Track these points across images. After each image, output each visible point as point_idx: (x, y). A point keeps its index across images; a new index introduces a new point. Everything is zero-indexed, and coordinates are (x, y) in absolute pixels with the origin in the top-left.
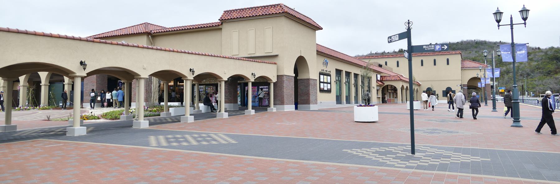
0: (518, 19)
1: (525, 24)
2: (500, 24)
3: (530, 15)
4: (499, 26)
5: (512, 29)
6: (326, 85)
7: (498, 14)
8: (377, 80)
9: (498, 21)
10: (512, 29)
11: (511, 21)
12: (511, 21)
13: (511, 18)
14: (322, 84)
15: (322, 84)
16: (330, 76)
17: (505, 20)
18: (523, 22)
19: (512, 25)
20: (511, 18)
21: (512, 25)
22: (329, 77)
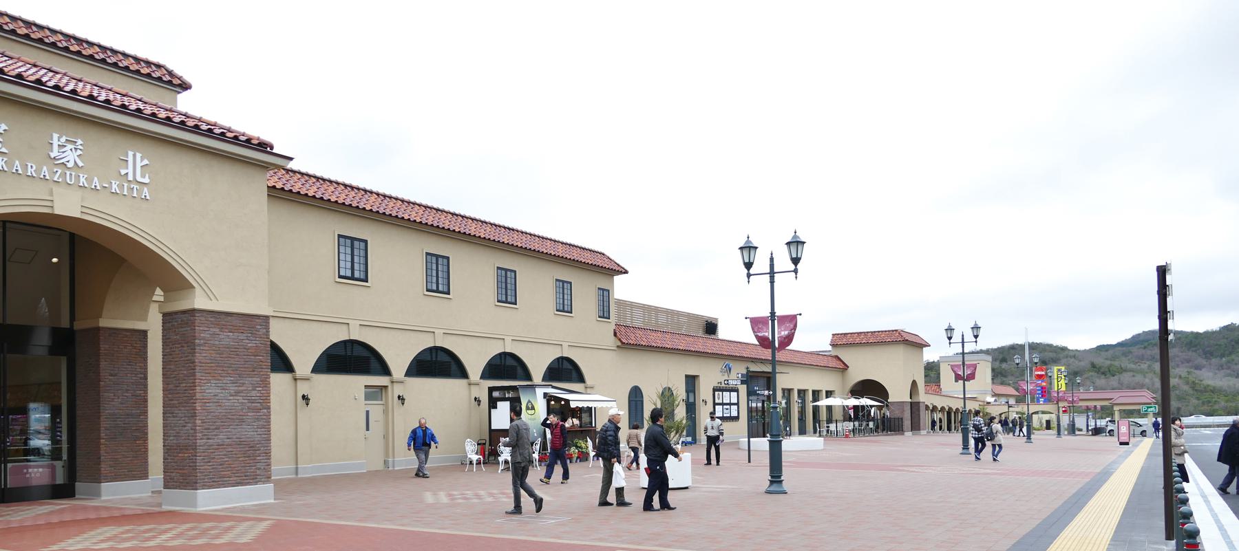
0: (783, 262)
1: (796, 271)
2: (752, 271)
3: (807, 254)
4: (749, 275)
5: (772, 282)
6: (726, 401)
7: (950, 330)
8: (816, 395)
9: (950, 338)
10: (772, 282)
11: (772, 266)
12: (772, 266)
13: (772, 259)
14: (734, 400)
15: (734, 400)
16: (737, 391)
17: (761, 264)
18: (792, 267)
19: (772, 273)
20: (772, 259)
21: (772, 273)
22: (734, 394)
